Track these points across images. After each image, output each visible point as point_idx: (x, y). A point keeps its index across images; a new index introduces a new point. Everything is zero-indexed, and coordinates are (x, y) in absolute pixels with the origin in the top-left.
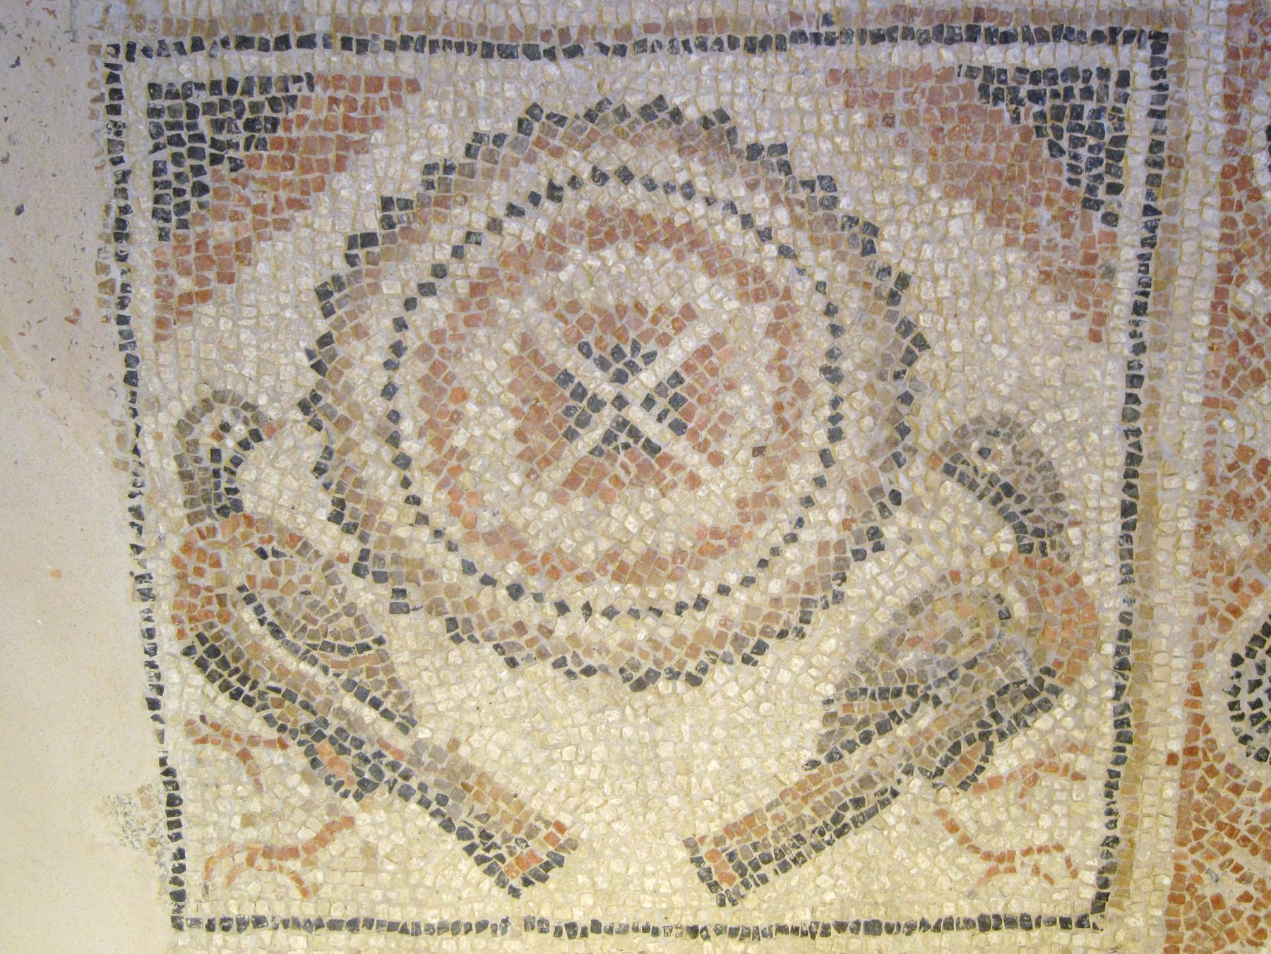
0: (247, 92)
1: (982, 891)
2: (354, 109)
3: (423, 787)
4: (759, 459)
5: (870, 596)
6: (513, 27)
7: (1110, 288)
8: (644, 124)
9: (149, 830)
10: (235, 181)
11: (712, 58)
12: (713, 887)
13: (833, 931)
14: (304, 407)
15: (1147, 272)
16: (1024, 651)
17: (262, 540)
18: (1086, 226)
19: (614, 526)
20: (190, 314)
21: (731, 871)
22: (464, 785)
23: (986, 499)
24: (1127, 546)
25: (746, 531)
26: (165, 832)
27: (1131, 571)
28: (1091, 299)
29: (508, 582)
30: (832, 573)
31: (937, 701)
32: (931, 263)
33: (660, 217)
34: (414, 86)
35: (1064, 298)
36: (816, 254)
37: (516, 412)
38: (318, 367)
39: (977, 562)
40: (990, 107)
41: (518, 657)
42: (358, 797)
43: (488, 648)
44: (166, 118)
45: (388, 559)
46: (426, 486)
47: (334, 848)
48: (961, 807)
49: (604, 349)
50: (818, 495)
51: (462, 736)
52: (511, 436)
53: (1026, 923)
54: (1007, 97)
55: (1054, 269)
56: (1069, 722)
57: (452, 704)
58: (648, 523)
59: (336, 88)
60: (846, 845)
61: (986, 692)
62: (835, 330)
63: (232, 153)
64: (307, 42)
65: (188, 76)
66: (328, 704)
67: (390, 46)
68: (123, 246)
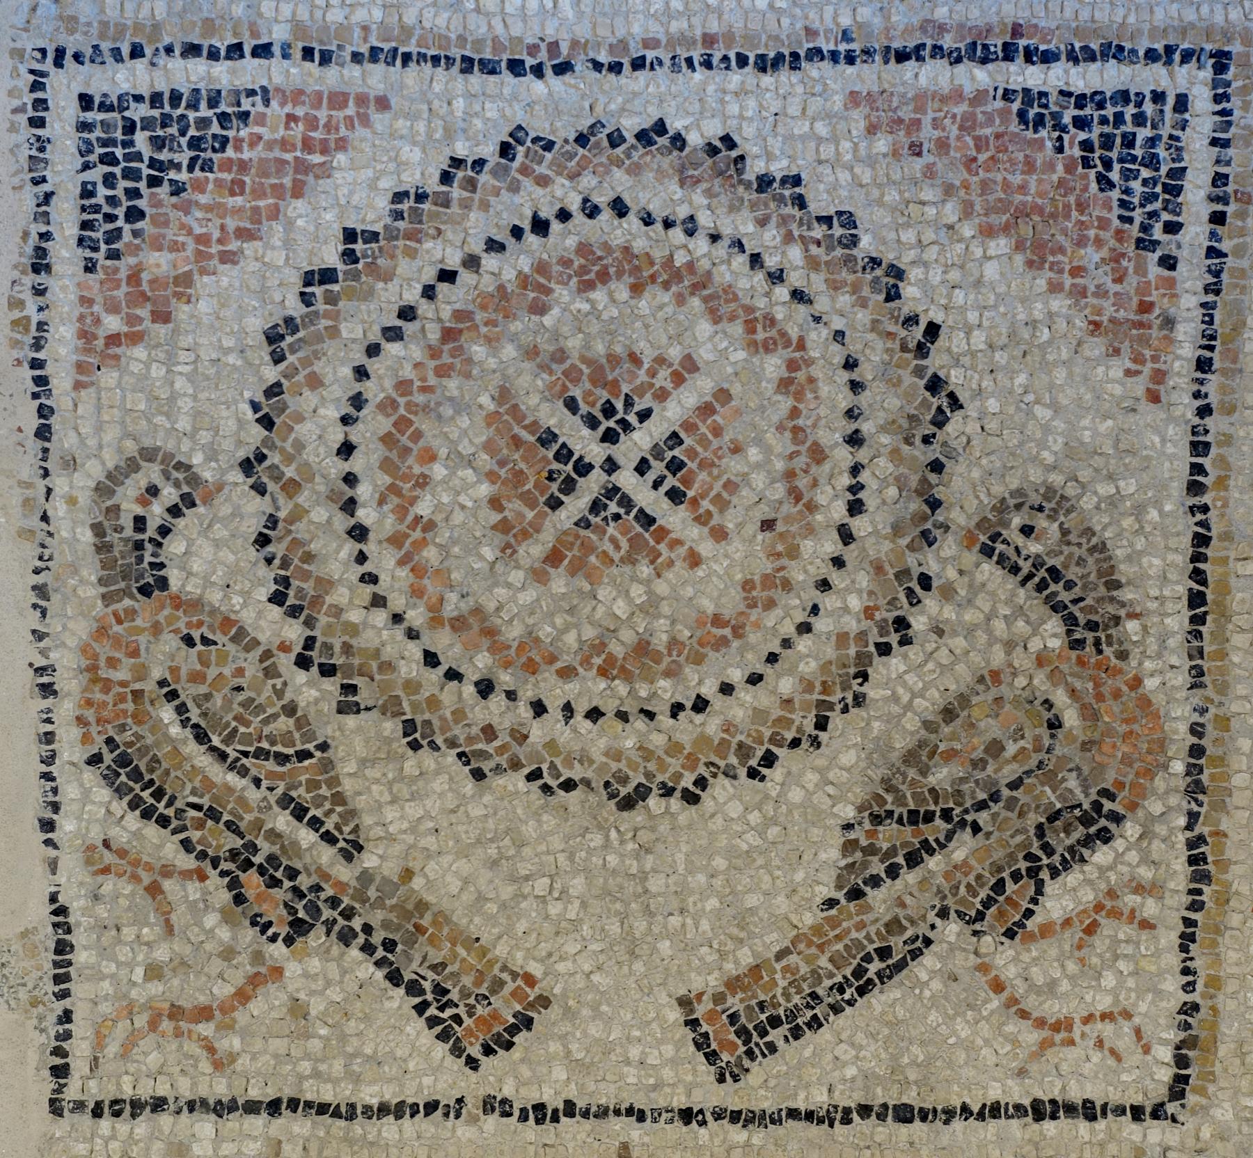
0: (193, 106)
1: (1034, 1068)
2: (316, 128)
3: (367, 929)
4: (768, 534)
5: (895, 698)
6: (495, 40)
7: (1170, 340)
8: (642, 151)
9: (30, 986)
10: (174, 206)
11: (717, 76)
12: (711, 1057)
13: (855, 1116)
14: (246, 467)
15: (1211, 322)
16: (1078, 769)
17: (189, 625)
18: (1141, 270)
19: (600, 611)
20: (117, 357)
21: (733, 1037)
22: (416, 926)
23: (1030, 585)
24: (1196, 643)
25: (753, 618)
26: (51, 988)
27: (1202, 674)
28: (1148, 353)
29: (476, 678)
30: (852, 671)
31: (976, 828)
32: (963, 310)
33: (658, 254)
34: (383, 103)
35: (1117, 352)
36: (833, 299)
37: (491, 476)
38: (267, 422)
39: (1022, 660)
40: (1030, 134)
41: (486, 766)
42: (289, 941)
43: (451, 757)
44: (98, 133)
45: (337, 649)
46: (384, 561)
47: (256, 1007)
48: (1006, 959)
49: (593, 405)
50: (835, 577)
51: (415, 865)
52: (484, 503)
53: (1089, 1111)
54: (1049, 123)
55: (1105, 319)
56: (1133, 856)
57: (405, 825)
58: (641, 608)
59: (295, 103)
60: (870, 1006)
61: (1034, 819)
62: (856, 386)
63: (172, 175)
64: (263, 51)
65: (125, 87)
66: (258, 825)
67: (357, 57)
68: (42, 278)
